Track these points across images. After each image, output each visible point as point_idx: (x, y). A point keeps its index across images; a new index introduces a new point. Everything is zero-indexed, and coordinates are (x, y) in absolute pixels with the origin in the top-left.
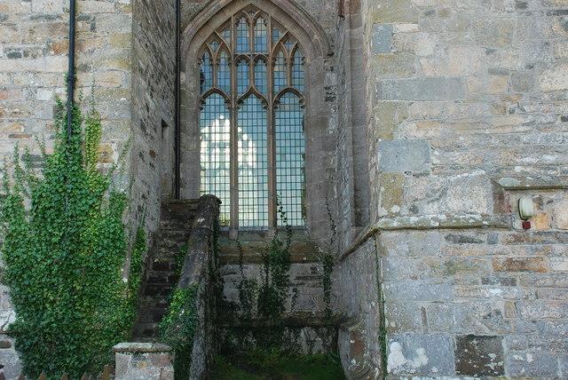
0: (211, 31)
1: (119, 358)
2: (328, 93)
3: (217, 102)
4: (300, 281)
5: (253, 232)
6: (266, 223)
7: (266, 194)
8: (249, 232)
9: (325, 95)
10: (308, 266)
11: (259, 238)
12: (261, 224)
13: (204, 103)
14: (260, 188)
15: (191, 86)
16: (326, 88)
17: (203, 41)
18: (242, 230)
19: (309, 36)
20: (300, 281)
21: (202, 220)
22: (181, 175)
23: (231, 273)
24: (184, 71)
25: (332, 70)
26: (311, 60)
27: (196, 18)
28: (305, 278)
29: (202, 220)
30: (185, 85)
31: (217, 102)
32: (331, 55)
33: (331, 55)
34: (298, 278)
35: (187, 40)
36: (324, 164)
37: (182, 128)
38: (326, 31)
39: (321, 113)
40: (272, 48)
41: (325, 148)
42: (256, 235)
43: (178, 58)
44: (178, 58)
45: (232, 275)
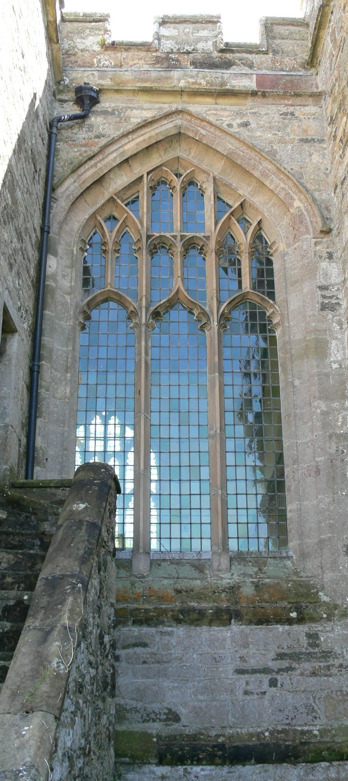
0: (107, 196)
1: (153, 557)
2: (324, 297)
3: (113, 315)
4: (285, 664)
5: (178, 562)
6: (207, 544)
7: (206, 487)
8: (172, 562)
9: (321, 300)
10: (300, 630)
11: (196, 574)
12: (196, 545)
13: (88, 318)
14: (195, 476)
15: (66, 283)
16: (322, 288)
17: (91, 211)
18: (156, 557)
19: (286, 205)
20: (285, 664)
21: (82, 506)
22: (39, 442)
23: (135, 645)
24: (55, 254)
25: (330, 256)
26: (288, 245)
27: (82, 170)
28: (296, 657)
29: (82, 506)
30: (54, 277)
31: (113, 315)
32: (327, 232)
33: (327, 232)
34: (281, 656)
35: (63, 204)
36: (326, 425)
37: (44, 352)
38: (316, 195)
39: (316, 330)
40: (216, 224)
41: (325, 396)
42: (187, 567)
43: (45, 230)
44: (45, 230)
45: (138, 650)
